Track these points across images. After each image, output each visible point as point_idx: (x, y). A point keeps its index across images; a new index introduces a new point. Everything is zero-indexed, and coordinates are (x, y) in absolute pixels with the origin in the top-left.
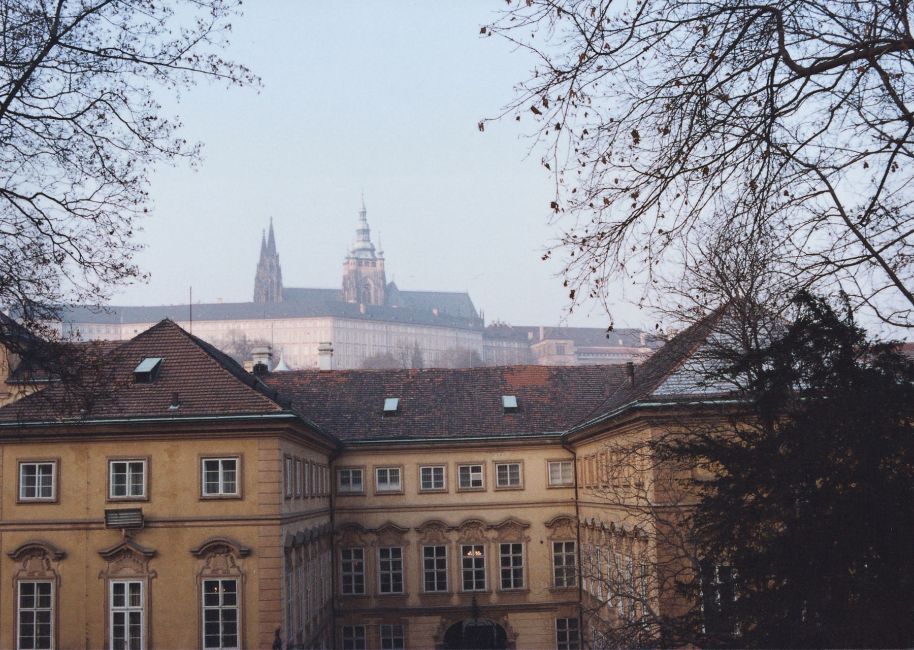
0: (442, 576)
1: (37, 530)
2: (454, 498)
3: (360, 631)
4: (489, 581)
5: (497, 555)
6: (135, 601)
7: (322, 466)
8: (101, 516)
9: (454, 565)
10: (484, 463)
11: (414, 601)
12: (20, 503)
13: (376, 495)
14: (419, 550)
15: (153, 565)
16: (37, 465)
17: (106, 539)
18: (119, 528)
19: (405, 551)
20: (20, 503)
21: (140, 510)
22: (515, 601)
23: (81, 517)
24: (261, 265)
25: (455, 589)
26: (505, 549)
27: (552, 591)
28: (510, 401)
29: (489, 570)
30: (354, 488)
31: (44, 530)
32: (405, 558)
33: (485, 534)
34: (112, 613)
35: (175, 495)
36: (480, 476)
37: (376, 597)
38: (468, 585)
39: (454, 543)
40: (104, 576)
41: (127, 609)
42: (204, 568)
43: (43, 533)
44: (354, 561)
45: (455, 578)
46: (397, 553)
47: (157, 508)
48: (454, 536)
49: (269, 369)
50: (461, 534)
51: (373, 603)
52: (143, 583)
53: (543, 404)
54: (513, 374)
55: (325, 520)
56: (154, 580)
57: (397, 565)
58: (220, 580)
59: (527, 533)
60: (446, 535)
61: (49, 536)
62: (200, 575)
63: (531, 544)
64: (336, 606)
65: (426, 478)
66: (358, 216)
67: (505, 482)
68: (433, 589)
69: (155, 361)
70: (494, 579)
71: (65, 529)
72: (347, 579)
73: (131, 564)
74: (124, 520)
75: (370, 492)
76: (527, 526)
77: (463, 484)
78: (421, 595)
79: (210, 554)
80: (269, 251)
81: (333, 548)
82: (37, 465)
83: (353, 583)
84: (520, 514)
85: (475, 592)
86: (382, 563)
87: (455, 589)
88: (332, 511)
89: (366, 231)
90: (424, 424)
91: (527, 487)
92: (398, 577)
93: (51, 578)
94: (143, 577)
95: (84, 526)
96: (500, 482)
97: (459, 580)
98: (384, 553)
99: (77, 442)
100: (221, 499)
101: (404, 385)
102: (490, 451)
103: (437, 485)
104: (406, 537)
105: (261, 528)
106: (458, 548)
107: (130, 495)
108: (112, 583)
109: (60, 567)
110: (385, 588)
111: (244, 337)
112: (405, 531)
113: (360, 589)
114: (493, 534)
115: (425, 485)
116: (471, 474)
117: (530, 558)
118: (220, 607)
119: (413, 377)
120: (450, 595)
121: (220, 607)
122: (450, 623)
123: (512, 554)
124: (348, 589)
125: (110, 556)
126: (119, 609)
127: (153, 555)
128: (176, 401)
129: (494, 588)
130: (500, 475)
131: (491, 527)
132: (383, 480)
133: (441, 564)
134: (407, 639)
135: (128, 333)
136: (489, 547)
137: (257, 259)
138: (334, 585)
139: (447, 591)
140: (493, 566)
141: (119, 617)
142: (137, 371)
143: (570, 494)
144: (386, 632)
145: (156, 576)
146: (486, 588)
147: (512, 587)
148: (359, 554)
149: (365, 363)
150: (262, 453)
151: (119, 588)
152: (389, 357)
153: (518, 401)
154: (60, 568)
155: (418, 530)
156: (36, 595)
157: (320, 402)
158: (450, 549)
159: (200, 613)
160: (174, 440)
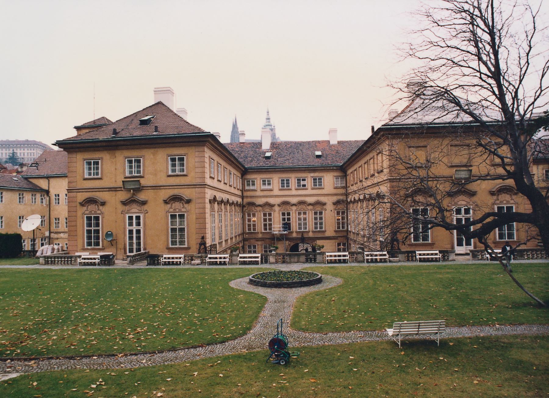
2: (294, 192)
4: (309, 227)
6: (138, 224)
8: (120, 184)
9: (294, 220)
12: (85, 179)
14: (279, 213)
15: (145, 207)
17: (123, 196)
18: (129, 190)
20: (85, 179)
21: (139, 181)
23: (112, 185)
24: (232, 132)
26: (316, 213)
27: (335, 231)
28: (319, 153)
30: (252, 187)
33: (308, 207)
34: (127, 230)
37: (261, 233)
41: (134, 228)
46: (270, 215)
48: (294, 208)
51: (260, 236)
57: (270, 220)
58: (177, 214)
59: (325, 207)
60: (291, 207)
63: (326, 212)
66: (266, 114)
75: (259, 190)
76: (324, 204)
79: (172, 202)
80: (235, 126)
81: (243, 212)
84: (323, 199)
89: (269, 119)
91: (325, 188)
95: (111, 189)
97: (296, 226)
98: (265, 215)
99: (110, 150)
100: (177, 176)
102: (310, 172)
103: (287, 186)
104: (273, 208)
106: (296, 213)
108: (127, 216)
110: (265, 229)
112: (273, 206)
113: (254, 229)
117: (326, 217)
120: (292, 232)
121: (93, 228)
122: (292, 244)
124: (249, 229)
125: (124, 203)
126: (131, 228)
127: (144, 203)
131: (310, 204)
136: (309, 213)
137: (231, 130)
138: (244, 228)
141: (131, 232)
143: (343, 191)
150: (197, 153)
151: (131, 218)
155: (279, 205)
159: (168, 230)
160: (155, 148)
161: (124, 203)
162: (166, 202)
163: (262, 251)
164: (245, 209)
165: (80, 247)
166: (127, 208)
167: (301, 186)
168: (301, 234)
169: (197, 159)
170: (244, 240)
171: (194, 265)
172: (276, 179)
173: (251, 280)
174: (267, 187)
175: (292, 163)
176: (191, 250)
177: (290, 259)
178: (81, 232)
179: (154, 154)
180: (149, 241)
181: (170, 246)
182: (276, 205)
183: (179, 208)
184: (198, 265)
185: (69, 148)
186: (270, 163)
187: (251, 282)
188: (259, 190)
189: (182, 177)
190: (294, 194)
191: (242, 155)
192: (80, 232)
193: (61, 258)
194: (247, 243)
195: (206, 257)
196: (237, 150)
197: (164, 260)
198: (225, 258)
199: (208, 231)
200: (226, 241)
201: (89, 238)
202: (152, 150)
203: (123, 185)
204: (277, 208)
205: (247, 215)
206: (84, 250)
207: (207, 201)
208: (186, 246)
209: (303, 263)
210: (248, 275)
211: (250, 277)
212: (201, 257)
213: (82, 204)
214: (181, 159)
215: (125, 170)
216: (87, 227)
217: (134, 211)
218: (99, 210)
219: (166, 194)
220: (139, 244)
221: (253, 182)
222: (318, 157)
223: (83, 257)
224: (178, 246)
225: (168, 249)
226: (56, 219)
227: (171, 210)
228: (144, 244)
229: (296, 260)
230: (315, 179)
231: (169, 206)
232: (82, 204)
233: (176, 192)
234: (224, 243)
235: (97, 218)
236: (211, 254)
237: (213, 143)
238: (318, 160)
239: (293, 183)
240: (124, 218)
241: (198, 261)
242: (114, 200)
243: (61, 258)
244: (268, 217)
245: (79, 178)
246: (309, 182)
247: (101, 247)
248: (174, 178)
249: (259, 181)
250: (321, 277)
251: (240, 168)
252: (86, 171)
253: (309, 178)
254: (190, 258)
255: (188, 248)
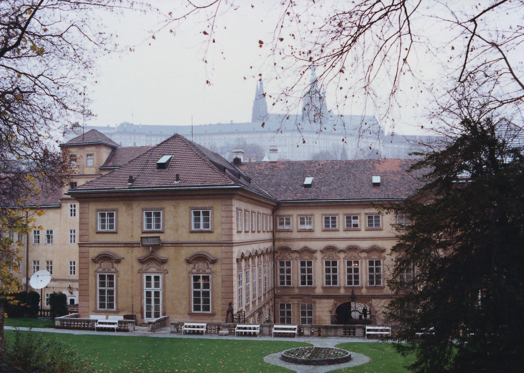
0: (335, 277)
1: (106, 247)
2: (342, 234)
3: (289, 306)
5: (366, 265)
6: (157, 285)
7: (267, 215)
9: (342, 272)
10: (359, 214)
11: (319, 291)
12: (98, 233)
13: (298, 232)
15: (165, 267)
16: (106, 213)
17: (139, 253)
18: (148, 246)
19: (314, 264)
20: (98, 233)
21: (159, 237)
22: (377, 293)
23: (129, 240)
25: (342, 285)
26: (371, 263)
28: (376, 179)
29: (362, 274)
30: (286, 227)
31: (110, 247)
32: (314, 267)
33: (360, 254)
34: (145, 292)
35: (177, 229)
36: (357, 222)
37: (298, 288)
38: (350, 283)
39: (342, 259)
40: (140, 272)
41: (153, 289)
42: (192, 269)
43: (110, 248)
44: (285, 267)
45: (342, 279)
46: (310, 263)
47: (167, 237)
48: (342, 255)
49: (242, 161)
50: (346, 254)
51: (296, 291)
52: (161, 276)
53: (395, 181)
54: (379, 164)
55: (269, 245)
56: (166, 275)
57: (310, 271)
58: (201, 275)
61: (113, 250)
62: (190, 272)
64: (276, 292)
65: (327, 222)
67: (372, 225)
68: (352, 284)
69: (169, 157)
70: (364, 279)
71: (121, 247)
72: (282, 278)
73: (154, 265)
74: (150, 242)
75: (295, 230)
76: (383, 251)
77: (347, 226)
78: (323, 288)
79: (196, 261)
81: (274, 260)
82: (106, 213)
83: (307, 280)
84: (380, 244)
85: (354, 287)
86: (301, 269)
87: (342, 285)
88: (274, 240)
90: (326, 192)
92: (310, 277)
93: (114, 273)
94: (161, 273)
95: (130, 245)
96: (369, 225)
97: (344, 280)
98: (303, 264)
100: (202, 232)
101: (317, 170)
102: (364, 208)
103: (333, 226)
104: (315, 255)
105: (223, 248)
107: (155, 229)
109: (118, 267)
110: (303, 283)
111: (245, 142)
112: (314, 252)
113: (289, 283)
114: (364, 255)
115: (326, 226)
116: (352, 220)
118: (201, 290)
119: (322, 165)
120: (339, 288)
121: (106, 288)
122: (339, 304)
123: (375, 266)
124: (282, 283)
125: (142, 261)
126: (149, 289)
127: (164, 262)
128: (177, 178)
129: (364, 285)
130: (369, 221)
131: (363, 251)
132: (302, 223)
133: (335, 270)
134: (315, 312)
135: (154, 142)
136: (362, 262)
139: (313, 286)
140: (364, 272)
141: (149, 294)
142: (158, 162)
144: (303, 307)
145: (167, 273)
146: (360, 285)
147: (286, 285)
148: (289, 264)
149: (314, 157)
151: (149, 278)
152: (328, 153)
153: (381, 179)
154: (118, 267)
155: (322, 252)
156: (107, 281)
157: (269, 179)
158: (340, 262)
160: (176, 200)
161: (142, 261)
162: (188, 262)
163: (298, 320)
164: (276, 255)
165: (92, 307)
166: (145, 266)
167: (351, 226)
168: (351, 290)
169: (224, 214)
170: (276, 297)
171: (221, 335)
172: (318, 217)
173: (283, 356)
174: (307, 227)
175: (339, 195)
176: (216, 317)
177: (326, 332)
178: (94, 292)
179: (175, 207)
180: (169, 305)
181: (193, 311)
182: (318, 252)
183: (203, 269)
184: (226, 335)
185: (81, 198)
186: (310, 195)
187: (284, 359)
188: (295, 230)
189: (207, 234)
190: (341, 237)
191: (274, 181)
192: (92, 293)
193: (74, 322)
194: (279, 302)
195: (235, 327)
196: (267, 173)
197: (185, 329)
198: (254, 329)
199: (236, 295)
200: (254, 303)
201: (102, 299)
202: (173, 202)
203: (141, 241)
204: (319, 255)
205: (278, 263)
206: (96, 312)
207: (234, 261)
208: (210, 312)
209: (342, 337)
210: (280, 351)
211: (283, 353)
212: (229, 327)
213: (95, 261)
214: (206, 214)
215: (142, 224)
216: (100, 286)
217: (153, 270)
218: (113, 267)
219: (187, 252)
220: (157, 308)
221: (288, 219)
222: (376, 185)
223: (99, 321)
224: (201, 311)
225: (191, 314)
226: (35, 262)
227: (195, 271)
228: (164, 307)
229: (333, 334)
230: (370, 217)
231: (192, 266)
232: (95, 261)
233: (199, 250)
234: (251, 306)
235: (111, 277)
236: (240, 324)
237: (242, 194)
238: (374, 190)
239: (341, 222)
240: (141, 277)
241: (225, 331)
242: (131, 257)
243: (74, 322)
244: (306, 267)
245: (91, 232)
246: (362, 221)
247: (115, 309)
248: (198, 235)
249: (295, 219)
250: (350, 355)
251: (269, 205)
252: (99, 224)
253: (362, 216)
254: (217, 327)
255: (213, 315)
